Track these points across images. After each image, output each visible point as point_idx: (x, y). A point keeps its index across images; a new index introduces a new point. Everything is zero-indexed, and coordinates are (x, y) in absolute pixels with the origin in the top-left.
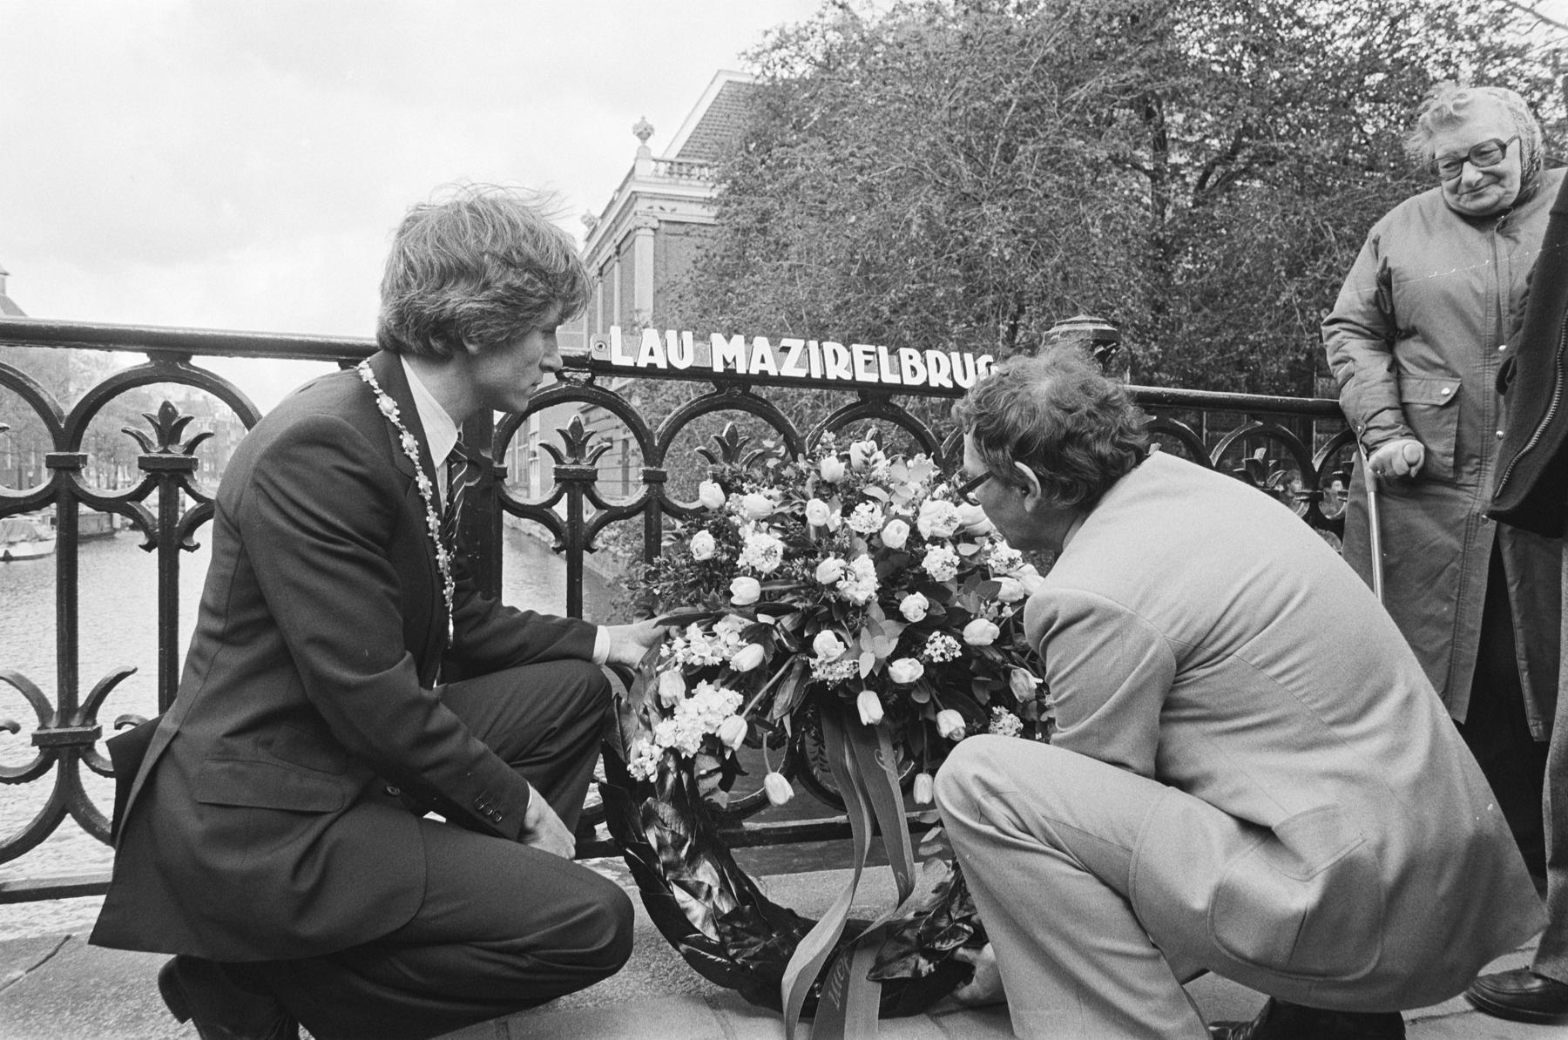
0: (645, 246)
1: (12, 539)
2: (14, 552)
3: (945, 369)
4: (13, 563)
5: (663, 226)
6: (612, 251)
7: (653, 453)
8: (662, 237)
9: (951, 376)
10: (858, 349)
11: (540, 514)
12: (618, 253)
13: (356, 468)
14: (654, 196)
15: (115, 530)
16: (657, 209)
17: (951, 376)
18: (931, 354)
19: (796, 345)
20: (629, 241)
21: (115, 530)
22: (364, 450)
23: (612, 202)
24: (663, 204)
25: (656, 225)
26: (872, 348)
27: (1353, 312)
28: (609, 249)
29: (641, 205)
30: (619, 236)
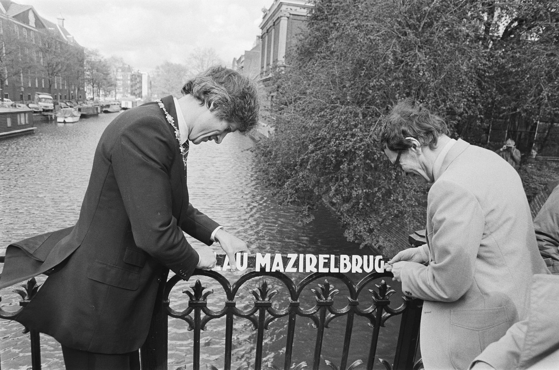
0: (284, 23)
1: (66, 116)
2: (67, 120)
3: (360, 264)
4: (67, 124)
5: (291, 16)
6: (272, 24)
7: (231, 295)
8: (290, 20)
9: (362, 267)
10: (321, 257)
11: (183, 316)
12: (274, 25)
13: (164, 139)
14: (289, 5)
15: (98, 113)
16: (289, 9)
17: (362, 267)
18: (354, 257)
19: (293, 257)
20: (277, 22)
21: (98, 113)
22: (167, 132)
23: (273, 4)
24: (292, 7)
25: (289, 15)
26: (328, 256)
27: (554, 233)
28: (271, 23)
29: (284, 8)
30: (275, 18)
